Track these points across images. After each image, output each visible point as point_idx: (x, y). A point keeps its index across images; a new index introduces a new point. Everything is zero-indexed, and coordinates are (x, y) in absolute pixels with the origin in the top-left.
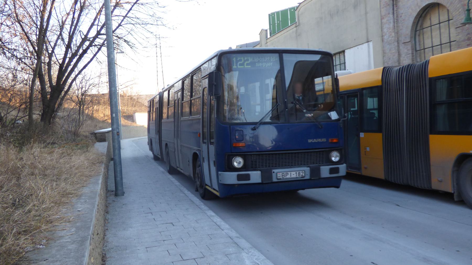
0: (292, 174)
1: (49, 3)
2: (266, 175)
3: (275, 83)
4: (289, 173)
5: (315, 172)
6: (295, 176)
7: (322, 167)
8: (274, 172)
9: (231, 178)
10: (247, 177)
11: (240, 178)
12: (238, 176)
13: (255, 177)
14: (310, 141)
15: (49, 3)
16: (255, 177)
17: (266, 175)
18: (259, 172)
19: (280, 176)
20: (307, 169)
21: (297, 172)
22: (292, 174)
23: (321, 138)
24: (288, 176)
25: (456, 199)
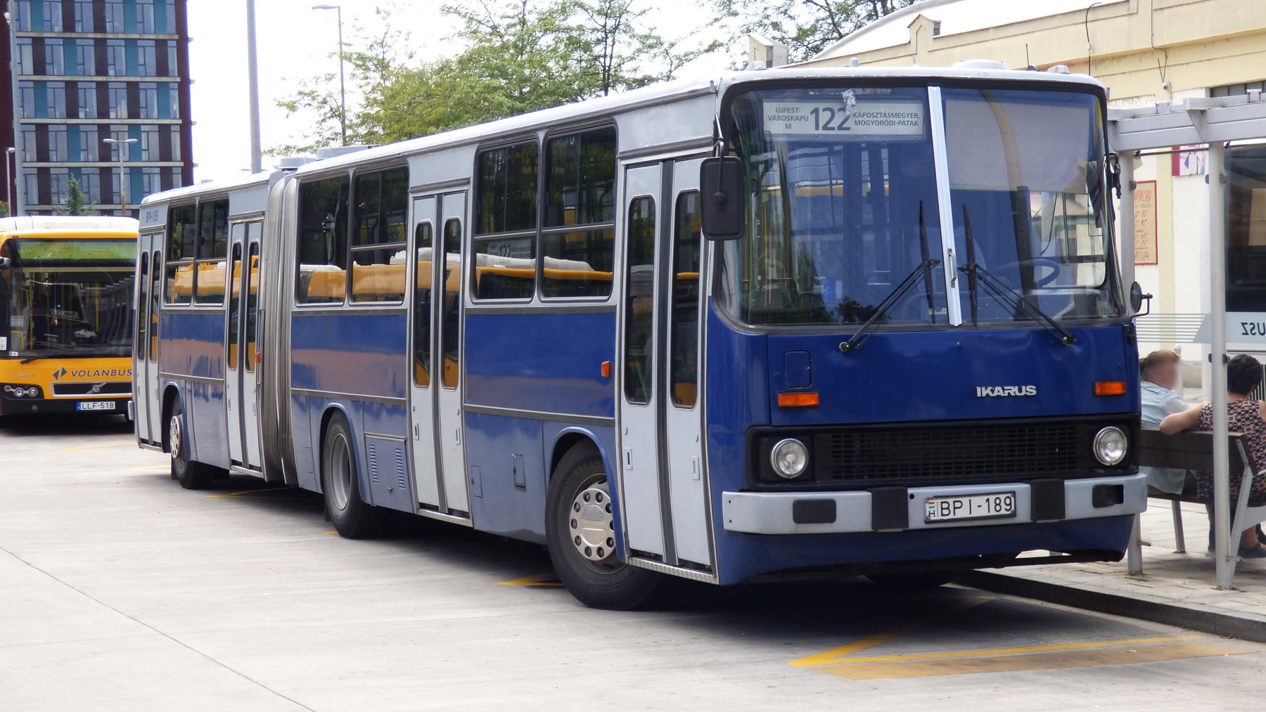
0: (977, 503)
1: (85, 12)
2: (890, 508)
3: (1171, 433)
4: (965, 500)
5: (1048, 501)
6: (983, 512)
7: (1068, 483)
8: (912, 496)
9: (752, 511)
10: (827, 511)
11: (802, 512)
12: (1097, 490)
13: (853, 510)
14: (982, 392)
15: (85, 12)
16: (853, 510)
17: (890, 508)
18: (865, 495)
19: (936, 512)
20: (1023, 489)
21: (992, 498)
22: (977, 503)
23: (1020, 383)
24: (962, 513)
25: (635, 269)
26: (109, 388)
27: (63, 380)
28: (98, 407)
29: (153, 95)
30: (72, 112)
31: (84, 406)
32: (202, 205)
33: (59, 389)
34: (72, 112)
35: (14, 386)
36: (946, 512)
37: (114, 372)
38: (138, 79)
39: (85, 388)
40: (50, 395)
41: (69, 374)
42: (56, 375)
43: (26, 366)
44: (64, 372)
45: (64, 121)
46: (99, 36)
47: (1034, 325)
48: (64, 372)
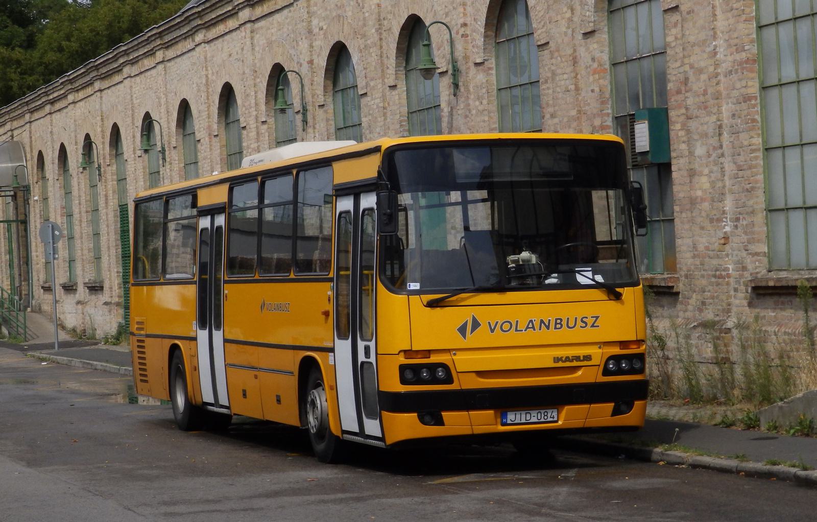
41: (483, 329)
48: (476, 324)
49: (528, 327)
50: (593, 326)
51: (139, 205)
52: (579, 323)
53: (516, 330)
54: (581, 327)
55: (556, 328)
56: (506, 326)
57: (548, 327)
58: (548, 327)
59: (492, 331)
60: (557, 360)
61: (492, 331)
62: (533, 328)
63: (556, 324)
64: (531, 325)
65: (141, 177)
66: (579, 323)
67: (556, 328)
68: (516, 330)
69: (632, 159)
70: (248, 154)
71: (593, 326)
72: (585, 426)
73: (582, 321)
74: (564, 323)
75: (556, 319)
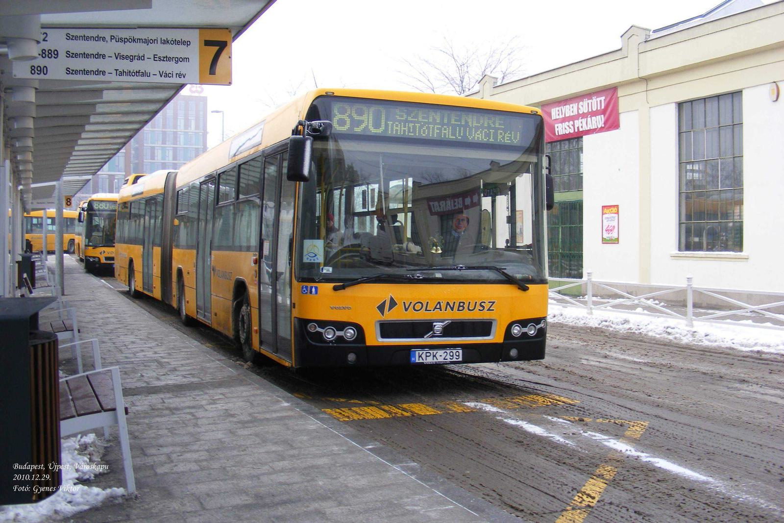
18: (367, 344)
26: (455, 328)
27: (391, 316)
28: (441, 356)
29: (160, 151)
30: (164, 142)
31: (422, 357)
32: (189, 191)
33: (387, 329)
34: (164, 142)
35: (323, 324)
36: (451, 354)
37: (461, 306)
38: (188, 146)
39: (421, 328)
40: (374, 338)
41: (400, 307)
42: (381, 308)
43: (341, 293)
44: (393, 303)
45: (172, 146)
46: (175, 130)
47: (540, 278)
48: (393, 303)
49: (436, 308)
50: (489, 310)
51: (527, 144)
52: (478, 307)
53: (426, 310)
54: (479, 310)
55: (458, 310)
56: (418, 306)
57: (452, 309)
58: (452, 309)
59: (406, 310)
60: (10, 223)
61: (406, 310)
62: (440, 309)
63: (459, 306)
64: (438, 306)
65: (359, 484)
66: (478, 307)
67: (458, 310)
68: (426, 310)
69: (43, 345)
70: (529, 420)
71: (489, 310)
72: (160, 276)
73: (481, 306)
74: (466, 306)
75: (460, 303)
